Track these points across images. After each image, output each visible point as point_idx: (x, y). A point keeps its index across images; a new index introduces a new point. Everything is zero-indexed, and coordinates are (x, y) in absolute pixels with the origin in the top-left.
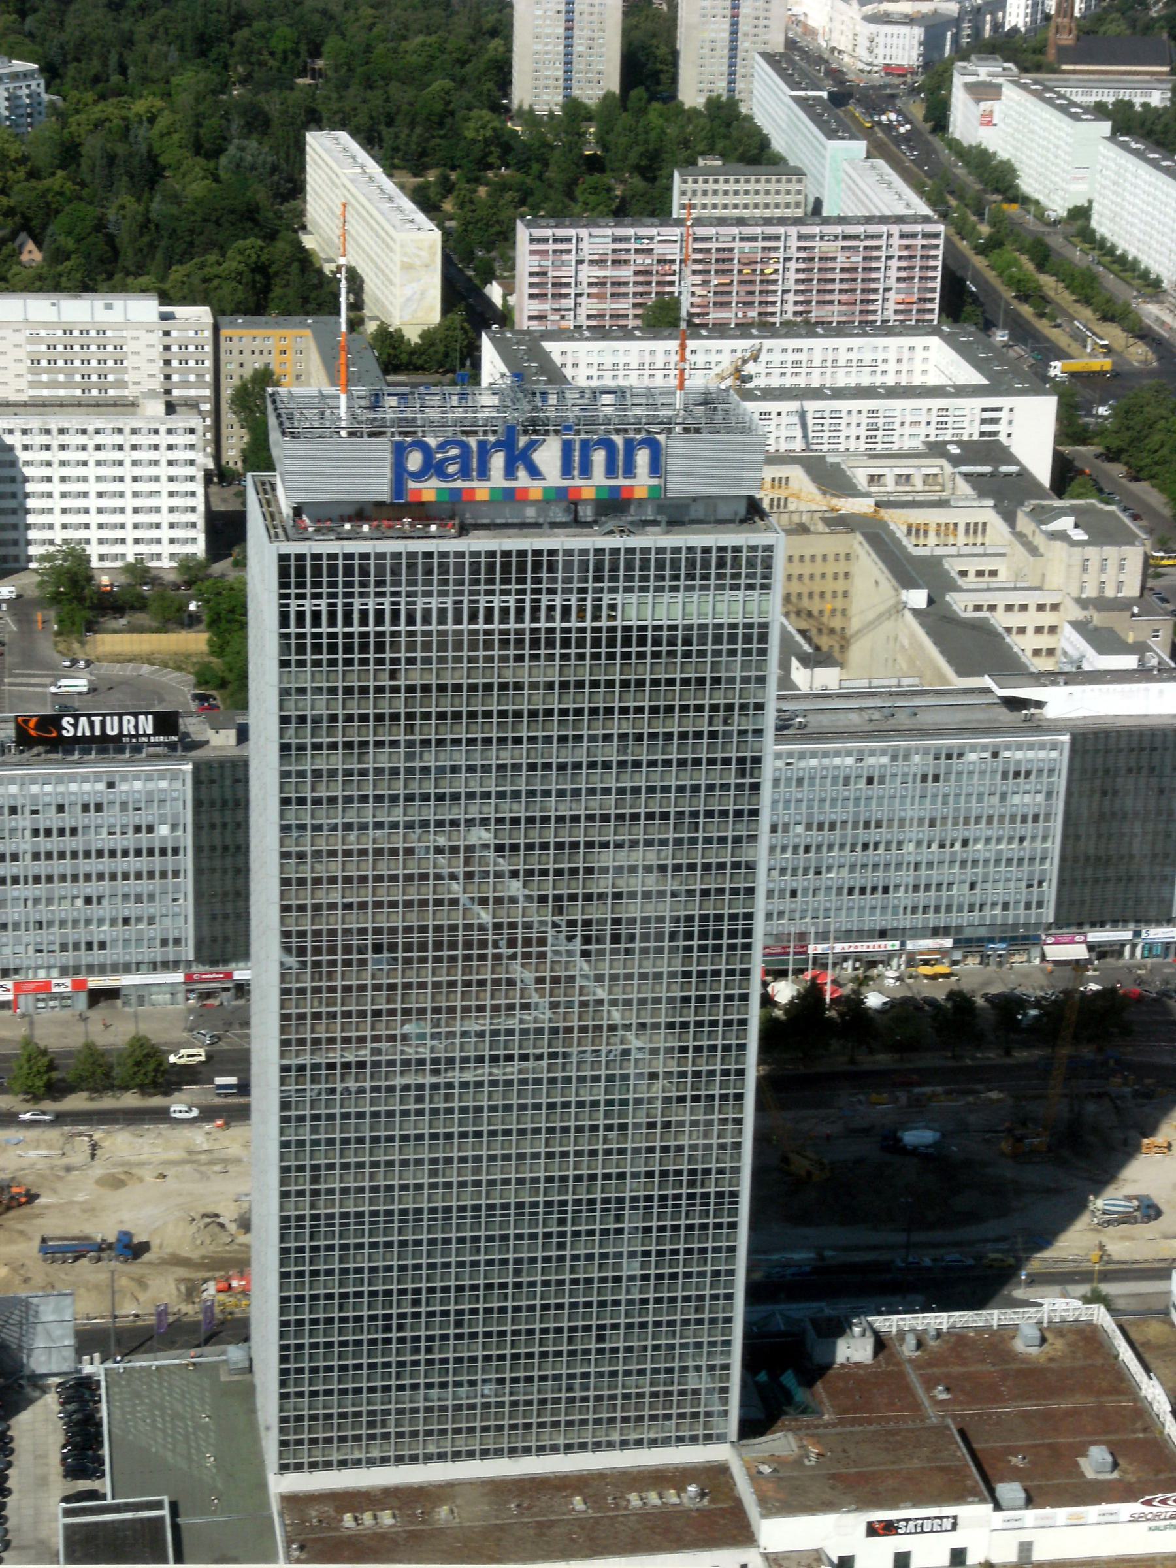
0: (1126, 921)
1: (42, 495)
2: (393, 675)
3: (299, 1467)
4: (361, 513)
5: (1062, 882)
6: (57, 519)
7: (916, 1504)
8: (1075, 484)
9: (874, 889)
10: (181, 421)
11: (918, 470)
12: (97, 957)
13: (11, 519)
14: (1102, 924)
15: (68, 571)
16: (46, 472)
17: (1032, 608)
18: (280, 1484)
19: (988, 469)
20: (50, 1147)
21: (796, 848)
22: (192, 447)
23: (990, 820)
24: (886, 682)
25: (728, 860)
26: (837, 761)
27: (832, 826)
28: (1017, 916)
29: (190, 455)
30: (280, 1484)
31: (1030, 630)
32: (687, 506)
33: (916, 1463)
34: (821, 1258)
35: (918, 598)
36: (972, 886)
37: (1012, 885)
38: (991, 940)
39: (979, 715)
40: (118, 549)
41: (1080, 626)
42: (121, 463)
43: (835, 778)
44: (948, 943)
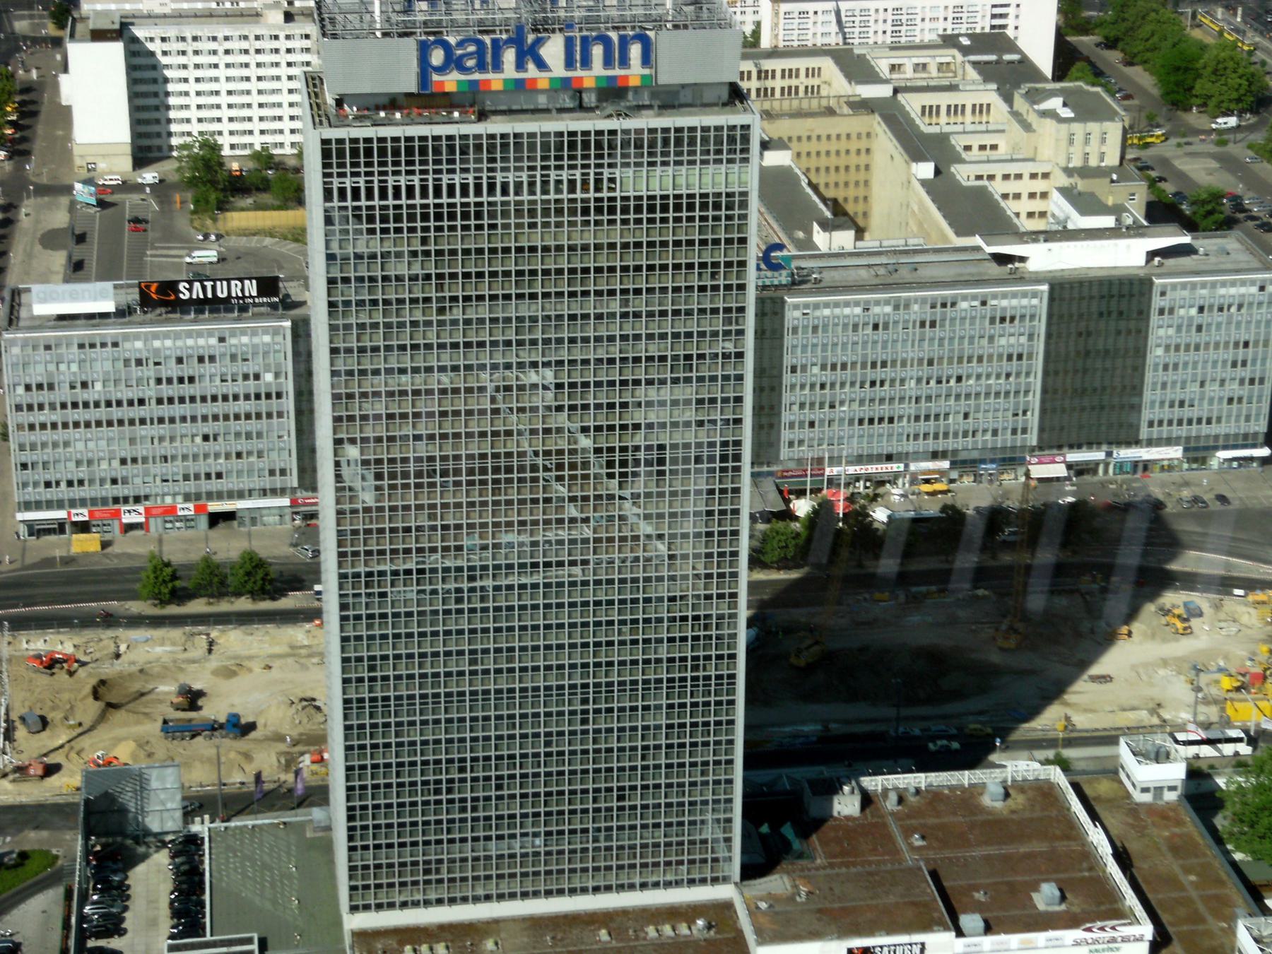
0: (1099, 444)
1: (180, 94)
2: (424, 241)
3: (367, 908)
4: (393, 103)
5: (1043, 411)
6: (194, 114)
7: (890, 931)
8: (1073, 70)
9: (881, 420)
10: (297, 28)
11: (934, 59)
12: (214, 485)
13: (155, 115)
14: (1079, 447)
15: (203, 158)
16: (182, 74)
17: (1026, 177)
18: (355, 922)
19: (993, 58)
20: (174, 644)
21: (812, 386)
22: (308, 50)
23: (980, 359)
24: (894, 242)
25: (719, 395)
26: (847, 311)
27: (844, 367)
28: (1005, 441)
29: (306, 57)
30: (355, 922)
31: (1025, 196)
32: (677, 93)
33: (892, 899)
34: (826, 729)
35: (926, 170)
36: (966, 416)
37: (1000, 414)
38: (983, 461)
39: (971, 269)
40: (246, 139)
41: (1066, 192)
42: (247, 65)
43: (845, 326)
44: (945, 464)
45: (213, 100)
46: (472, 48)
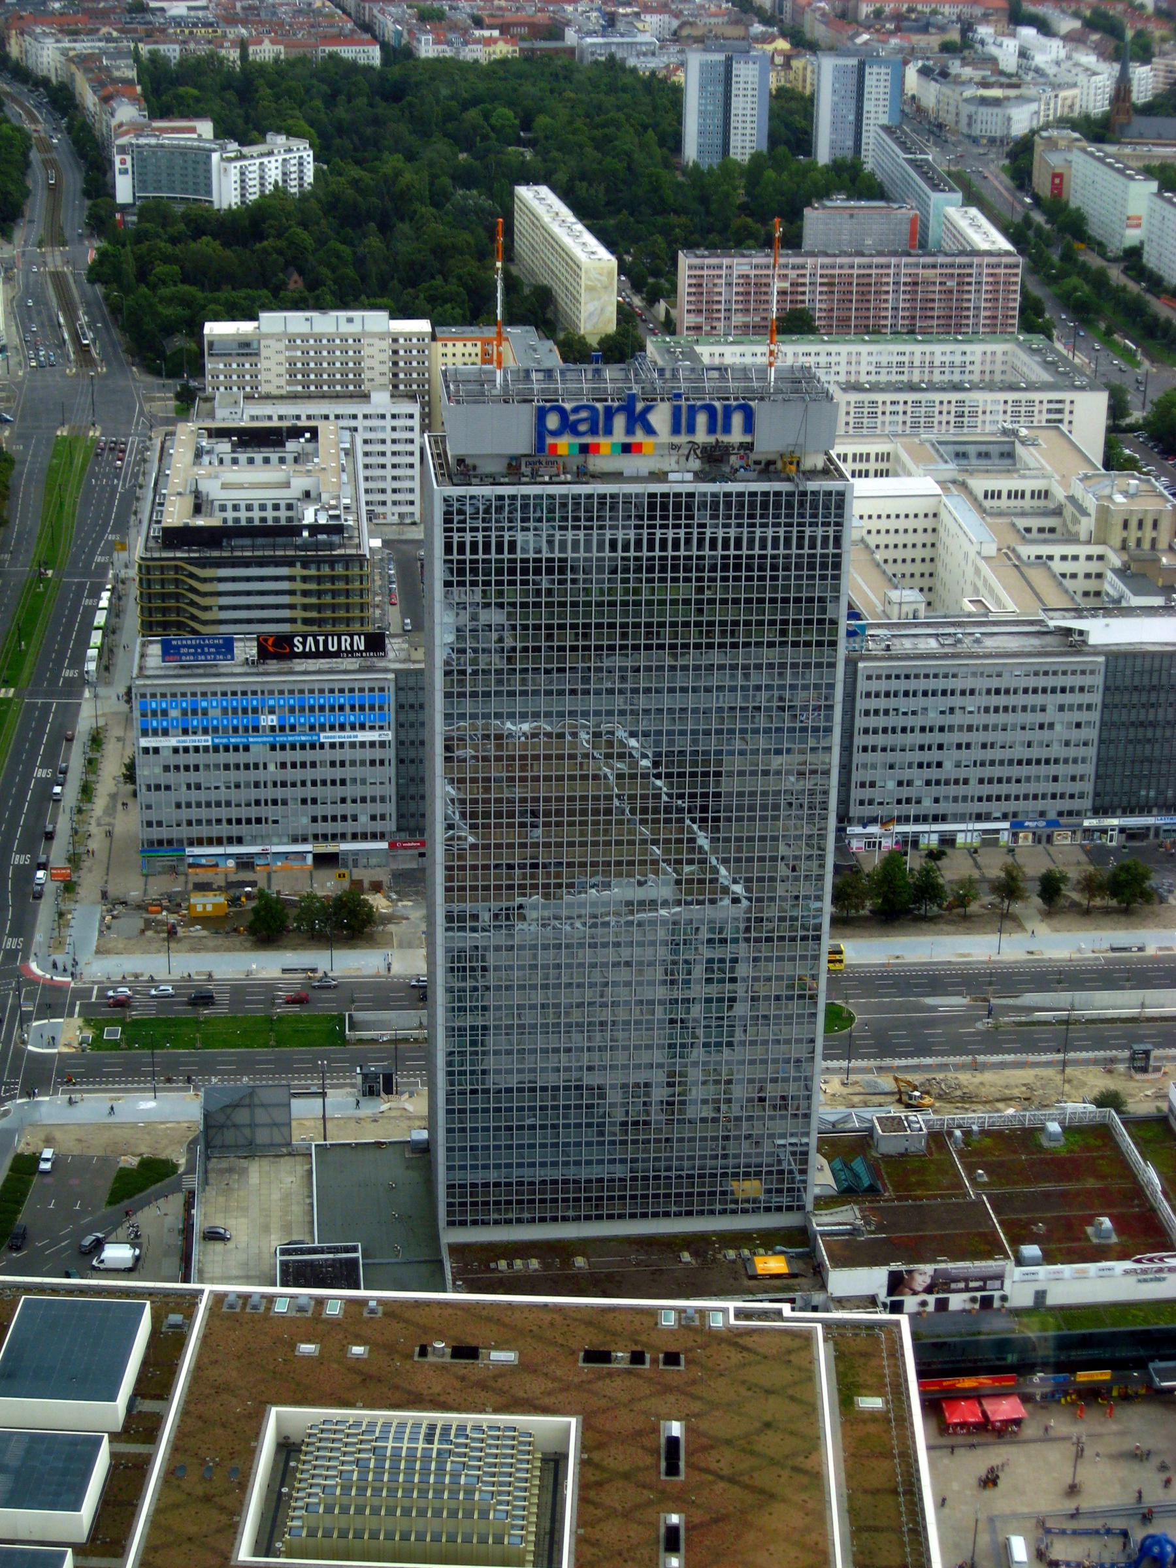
3: (463, 1223)
18: (451, 1236)
30: (451, 1236)
46: (584, 414)
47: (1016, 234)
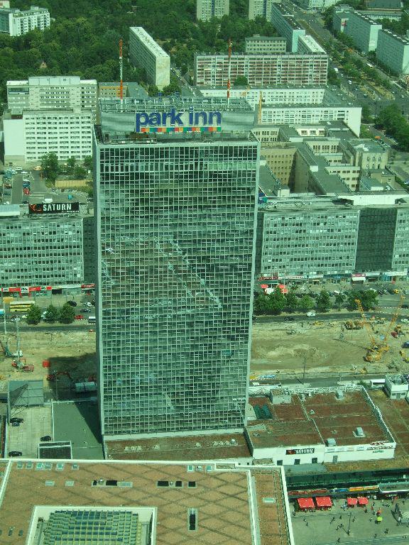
22: (89, 122)
31: (351, 179)
40: (66, 155)
45: (62, 145)
47: (327, 48)
